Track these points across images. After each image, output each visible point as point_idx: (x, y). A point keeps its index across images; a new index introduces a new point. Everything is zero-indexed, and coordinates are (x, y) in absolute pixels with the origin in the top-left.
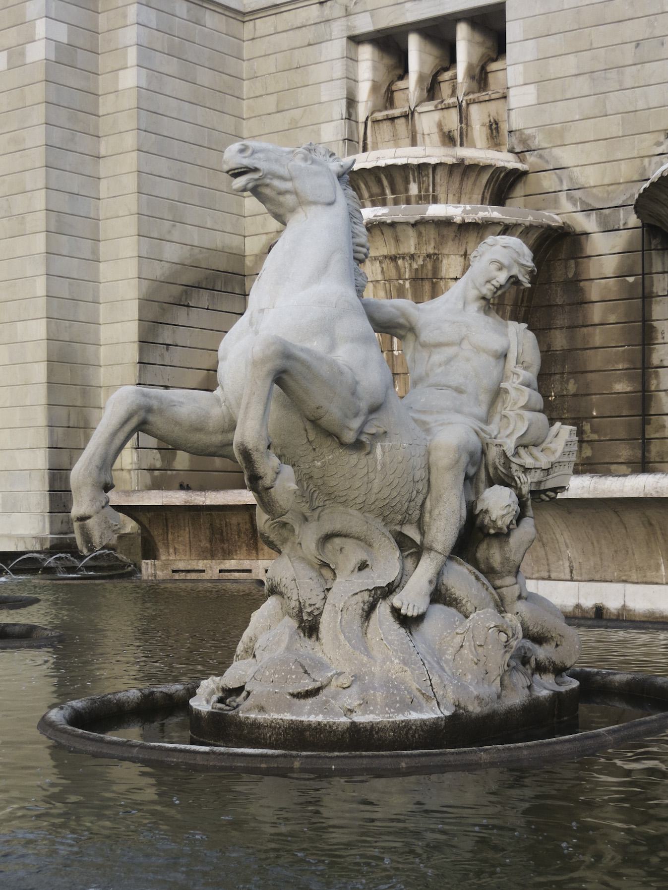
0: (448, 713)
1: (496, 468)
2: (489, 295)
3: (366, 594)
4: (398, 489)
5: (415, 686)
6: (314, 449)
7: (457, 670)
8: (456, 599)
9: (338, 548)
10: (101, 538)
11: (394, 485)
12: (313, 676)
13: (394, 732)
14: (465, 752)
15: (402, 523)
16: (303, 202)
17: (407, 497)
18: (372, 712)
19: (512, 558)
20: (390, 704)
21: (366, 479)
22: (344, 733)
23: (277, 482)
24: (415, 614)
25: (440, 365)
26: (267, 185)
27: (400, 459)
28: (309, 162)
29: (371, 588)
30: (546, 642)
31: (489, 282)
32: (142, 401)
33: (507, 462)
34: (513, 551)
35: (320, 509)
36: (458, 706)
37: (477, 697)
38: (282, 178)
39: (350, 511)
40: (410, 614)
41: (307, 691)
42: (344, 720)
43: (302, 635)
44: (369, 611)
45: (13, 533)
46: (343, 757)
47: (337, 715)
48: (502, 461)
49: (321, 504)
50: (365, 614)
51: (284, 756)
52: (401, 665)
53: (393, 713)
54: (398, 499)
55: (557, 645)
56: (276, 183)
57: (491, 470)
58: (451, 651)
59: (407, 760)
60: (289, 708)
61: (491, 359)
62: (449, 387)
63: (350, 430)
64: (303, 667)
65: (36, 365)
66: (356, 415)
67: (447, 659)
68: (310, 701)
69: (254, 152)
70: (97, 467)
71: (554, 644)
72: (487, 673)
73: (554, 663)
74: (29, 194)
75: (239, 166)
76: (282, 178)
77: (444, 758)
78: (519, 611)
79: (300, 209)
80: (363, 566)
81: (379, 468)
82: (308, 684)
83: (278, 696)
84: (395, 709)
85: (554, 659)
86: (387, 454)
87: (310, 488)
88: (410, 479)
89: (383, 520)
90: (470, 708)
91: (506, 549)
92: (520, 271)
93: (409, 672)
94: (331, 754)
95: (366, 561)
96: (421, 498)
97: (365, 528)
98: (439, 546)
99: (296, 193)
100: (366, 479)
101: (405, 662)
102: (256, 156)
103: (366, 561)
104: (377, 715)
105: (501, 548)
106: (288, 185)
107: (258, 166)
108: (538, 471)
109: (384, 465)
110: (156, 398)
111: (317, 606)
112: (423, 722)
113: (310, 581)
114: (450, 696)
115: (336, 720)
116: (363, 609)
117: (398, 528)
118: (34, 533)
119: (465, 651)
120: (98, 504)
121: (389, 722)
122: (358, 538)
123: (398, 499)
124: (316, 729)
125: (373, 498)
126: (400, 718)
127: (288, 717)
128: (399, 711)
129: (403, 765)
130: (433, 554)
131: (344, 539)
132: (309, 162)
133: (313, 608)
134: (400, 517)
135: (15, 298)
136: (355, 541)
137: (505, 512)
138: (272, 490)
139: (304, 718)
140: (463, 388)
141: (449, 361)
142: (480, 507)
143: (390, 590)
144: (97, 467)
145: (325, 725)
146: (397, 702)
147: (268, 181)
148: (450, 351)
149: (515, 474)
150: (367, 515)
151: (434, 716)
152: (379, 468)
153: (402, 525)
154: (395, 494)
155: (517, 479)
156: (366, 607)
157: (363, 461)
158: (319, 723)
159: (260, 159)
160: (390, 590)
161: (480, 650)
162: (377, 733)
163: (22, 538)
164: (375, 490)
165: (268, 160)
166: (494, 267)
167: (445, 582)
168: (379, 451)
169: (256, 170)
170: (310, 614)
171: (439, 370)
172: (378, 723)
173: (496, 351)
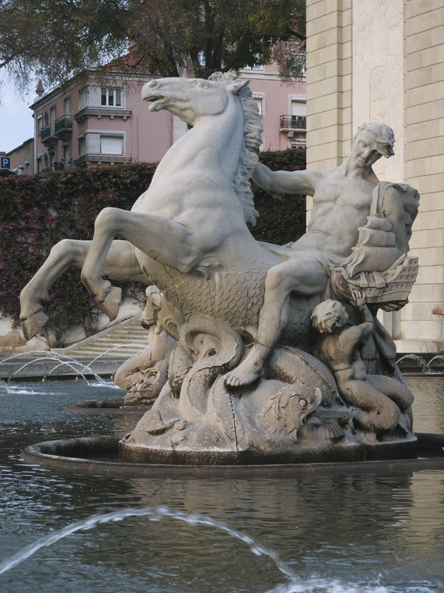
0: (241, 449)
1: (337, 288)
2: (360, 164)
3: (207, 370)
4: (234, 303)
5: (223, 431)
6: (171, 277)
7: (265, 422)
8: (288, 377)
9: (200, 340)
10: (31, 331)
11: (230, 299)
12: (163, 421)
13: (199, 459)
14: (186, 467)
15: (244, 324)
16: (197, 115)
17: (243, 307)
18: (188, 445)
19: (341, 350)
20: (201, 440)
21: (209, 296)
22: (169, 457)
23: (107, 298)
24: (236, 384)
25: (320, 216)
26: (172, 106)
27: (234, 282)
28: (206, 87)
29: (210, 366)
30: (371, 410)
31: (359, 155)
32: (70, 248)
33: (345, 284)
34: (342, 345)
35: (188, 315)
36: (252, 446)
37: (269, 441)
38: (181, 100)
39: (206, 316)
40: (232, 384)
41: (157, 431)
42: (170, 449)
43: (173, 396)
44: (210, 382)
45: (420, 338)
46: (113, 465)
47: (167, 446)
48: (341, 283)
49: (189, 312)
50: (207, 384)
51: (86, 463)
52: (217, 417)
53: (200, 447)
54: (236, 309)
55: (379, 413)
56: (178, 104)
57: (334, 289)
58: (264, 410)
59: (148, 469)
60: (146, 441)
61: (354, 211)
62: (321, 231)
63: (184, 264)
64: (160, 415)
65: (438, 194)
66: (188, 254)
67: (259, 416)
68: (159, 437)
69: (161, 85)
70: (34, 289)
71: (376, 412)
72: (286, 426)
73: (374, 425)
74: (435, 48)
75: (149, 96)
76: (181, 100)
77: (172, 470)
78: (350, 388)
79: (197, 119)
80: (212, 353)
81: (217, 288)
82: (159, 426)
83: (141, 432)
84: (203, 444)
85: (374, 422)
86: (223, 279)
87: (180, 301)
88: (244, 295)
89: (230, 322)
90: (262, 448)
91: (337, 344)
92: (378, 147)
93: (221, 422)
94: (108, 463)
95: (214, 349)
96: (256, 308)
97: (214, 327)
98: (262, 340)
99: (191, 109)
100: (209, 296)
101: (220, 415)
102: (163, 88)
103: (214, 349)
104: (190, 447)
105: (334, 343)
106: (187, 105)
107: (163, 94)
108: (374, 290)
109: (221, 287)
110: (82, 246)
111: (181, 378)
112: (220, 454)
113: (180, 361)
114: (247, 439)
115: (165, 449)
116: (205, 380)
117: (242, 328)
118: (435, 338)
119: (272, 411)
120: (31, 311)
121: (195, 452)
122: (211, 334)
123: (236, 309)
124: (155, 454)
125: (217, 308)
126: (205, 450)
127: (143, 446)
128: (207, 446)
129: (145, 472)
130: (258, 345)
131: (204, 335)
132: (206, 87)
133: (178, 378)
134: (241, 320)
135: (424, 138)
136: (211, 336)
137: (326, 318)
138: (104, 303)
139: (150, 447)
140: (329, 231)
141: (325, 213)
142: (314, 314)
143: (227, 368)
144: (34, 289)
145: (159, 452)
146: (205, 440)
147: (172, 103)
148: (327, 205)
149: (352, 291)
150: (217, 319)
151: (230, 450)
152: (217, 288)
153: (245, 326)
154: (233, 305)
155: (353, 295)
156: (207, 379)
157: (206, 284)
158: (156, 450)
159: (165, 90)
160: (227, 368)
161: (283, 411)
162: (188, 459)
163: (425, 342)
164: (217, 303)
165: (172, 89)
166: (361, 144)
167: (278, 365)
168: (217, 277)
169: (162, 97)
170: (176, 382)
171: (319, 220)
172: (189, 452)
173: (357, 204)
